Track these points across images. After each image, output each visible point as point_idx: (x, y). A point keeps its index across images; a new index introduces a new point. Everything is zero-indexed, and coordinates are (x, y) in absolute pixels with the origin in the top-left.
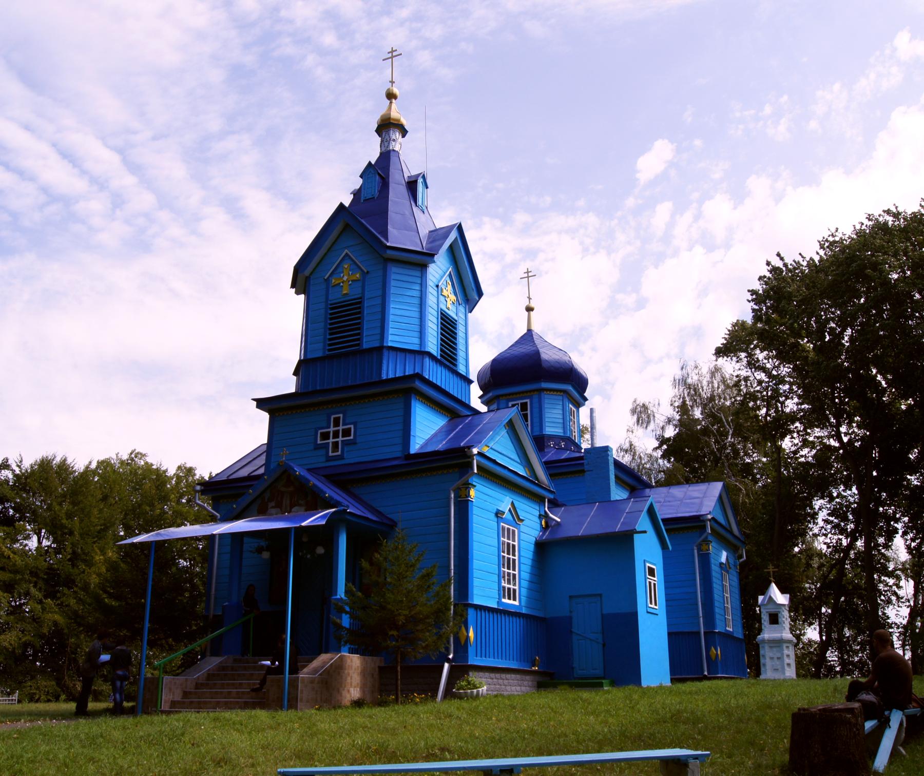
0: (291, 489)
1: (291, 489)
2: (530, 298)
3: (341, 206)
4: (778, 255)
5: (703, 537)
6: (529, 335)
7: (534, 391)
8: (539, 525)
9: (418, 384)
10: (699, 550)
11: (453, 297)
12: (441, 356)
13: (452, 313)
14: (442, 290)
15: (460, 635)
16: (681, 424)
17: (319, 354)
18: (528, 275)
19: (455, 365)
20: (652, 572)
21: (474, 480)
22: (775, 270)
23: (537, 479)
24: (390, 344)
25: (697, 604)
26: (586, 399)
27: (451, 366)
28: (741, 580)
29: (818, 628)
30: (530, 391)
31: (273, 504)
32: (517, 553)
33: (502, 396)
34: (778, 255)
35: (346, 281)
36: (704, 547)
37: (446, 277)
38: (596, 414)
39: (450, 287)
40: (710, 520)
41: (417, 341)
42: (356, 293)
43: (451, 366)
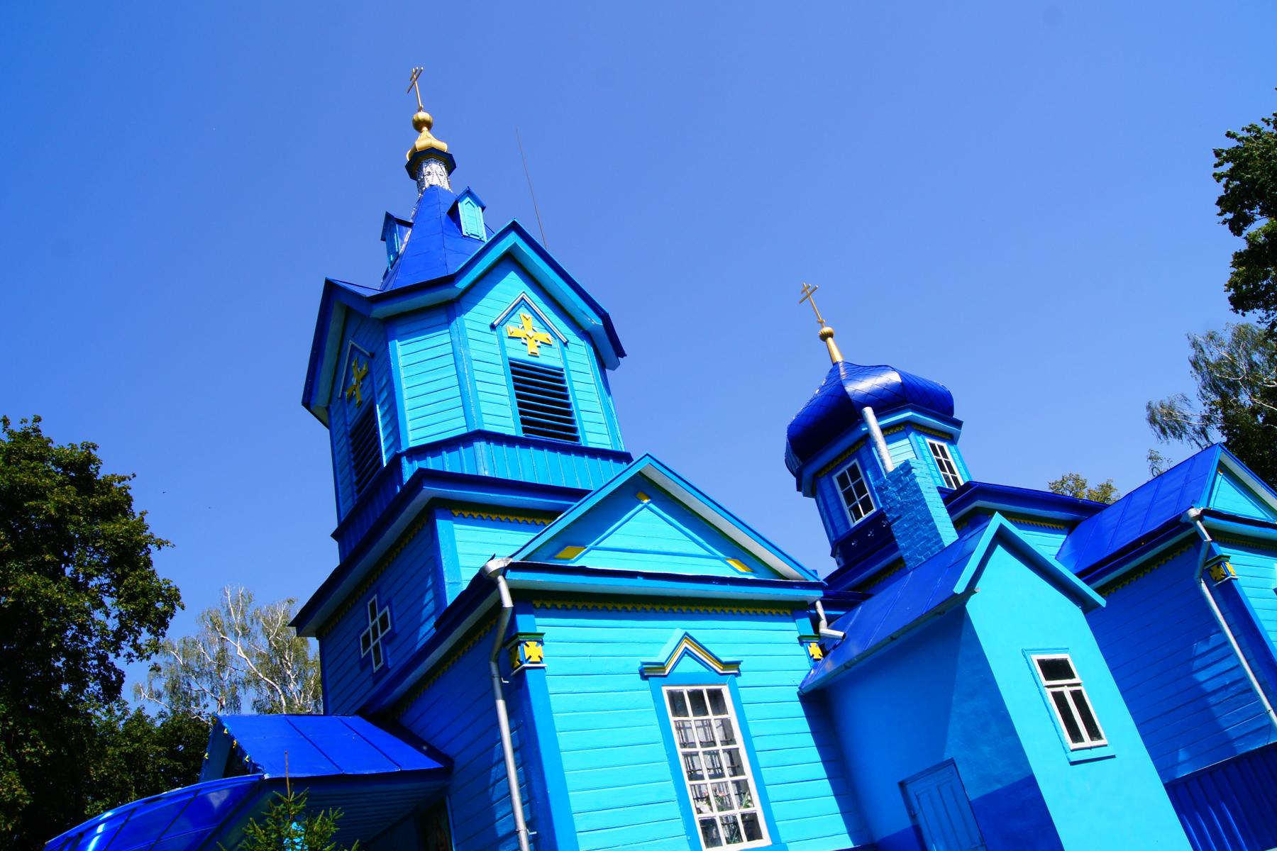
4: (1228, 135)
5: (1203, 552)
7: (857, 443)
8: (806, 659)
9: (431, 491)
12: (525, 430)
13: (550, 358)
16: (1229, 426)
20: (1055, 669)
21: (525, 623)
22: (1232, 155)
23: (781, 576)
24: (412, 445)
25: (1250, 689)
26: (958, 424)
27: (569, 442)
30: (853, 446)
32: (738, 735)
33: (820, 471)
34: (1228, 135)
40: (1200, 517)
43: (569, 442)
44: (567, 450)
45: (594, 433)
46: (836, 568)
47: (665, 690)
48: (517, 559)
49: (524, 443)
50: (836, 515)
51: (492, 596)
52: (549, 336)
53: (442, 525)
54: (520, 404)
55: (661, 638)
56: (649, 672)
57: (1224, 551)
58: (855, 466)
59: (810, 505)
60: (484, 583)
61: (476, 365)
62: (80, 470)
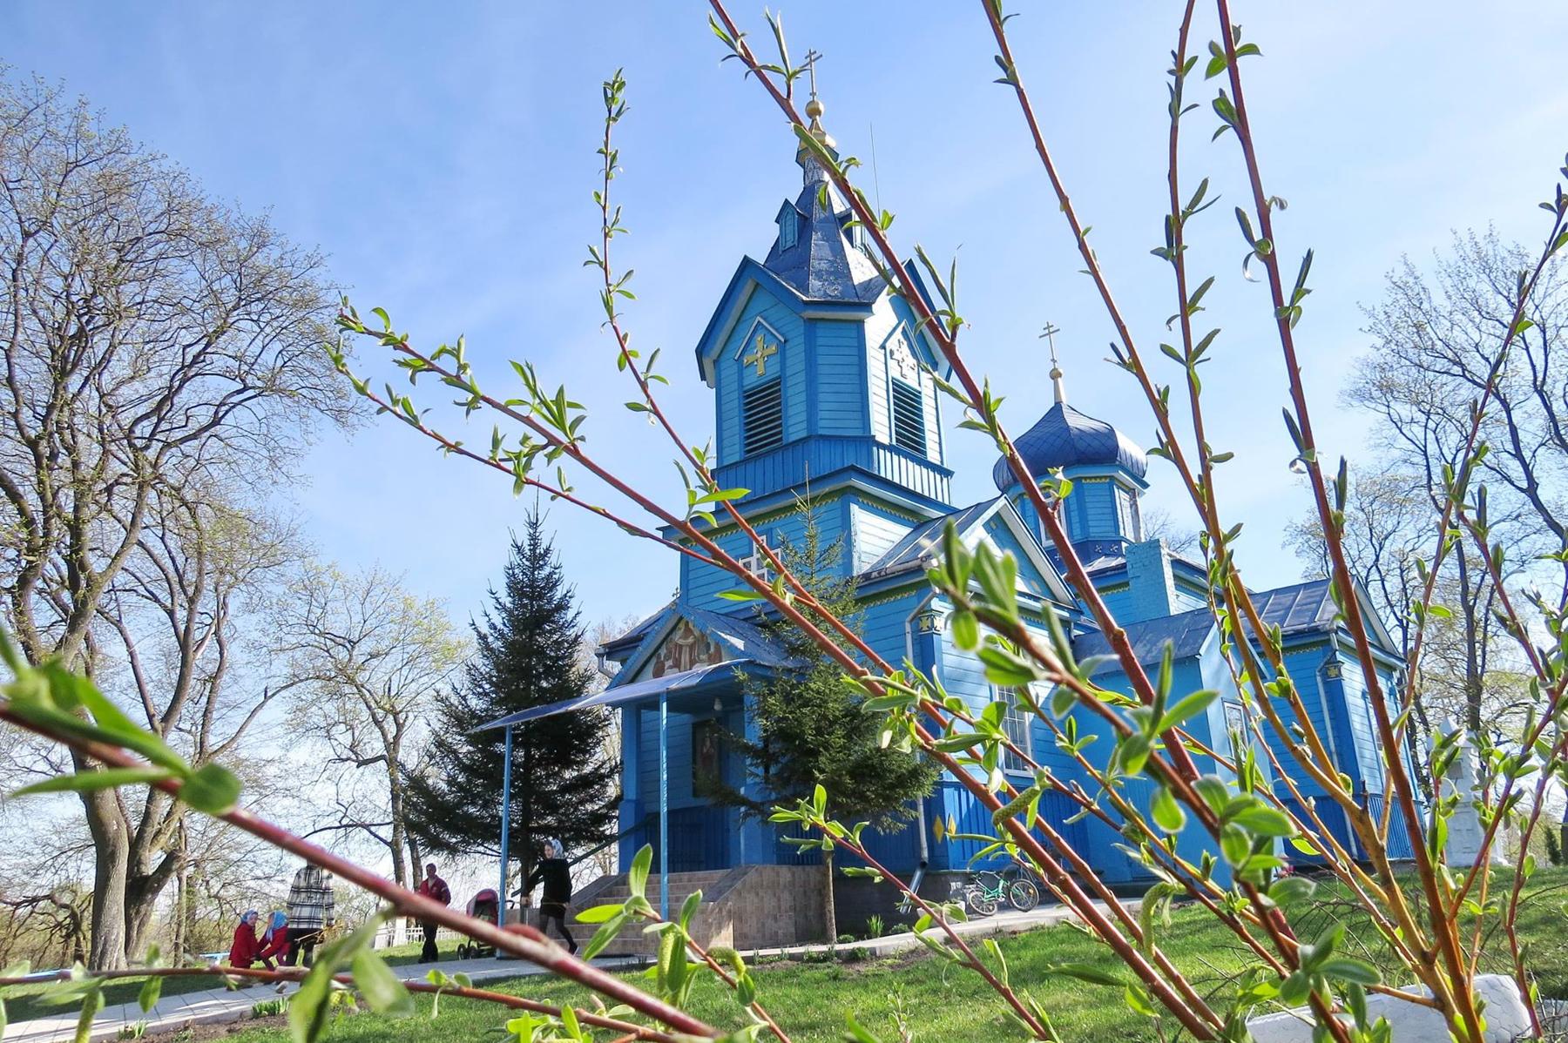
0: (691, 640)
1: (691, 640)
2: (1054, 361)
3: (747, 263)
6: (1056, 411)
10: (1325, 676)
11: (911, 361)
13: (911, 381)
14: (892, 352)
15: (936, 829)
17: (736, 458)
18: (1049, 331)
19: (924, 453)
24: (821, 432)
26: (1146, 485)
28: (849, 542)
29: (856, 562)
31: (669, 663)
35: (760, 362)
36: (1333, 672)
37: (898, 334)
38: (659, 355)
39: (905, 347)
41: (858, 424)
42: (774, 371)
49: (899, 452)
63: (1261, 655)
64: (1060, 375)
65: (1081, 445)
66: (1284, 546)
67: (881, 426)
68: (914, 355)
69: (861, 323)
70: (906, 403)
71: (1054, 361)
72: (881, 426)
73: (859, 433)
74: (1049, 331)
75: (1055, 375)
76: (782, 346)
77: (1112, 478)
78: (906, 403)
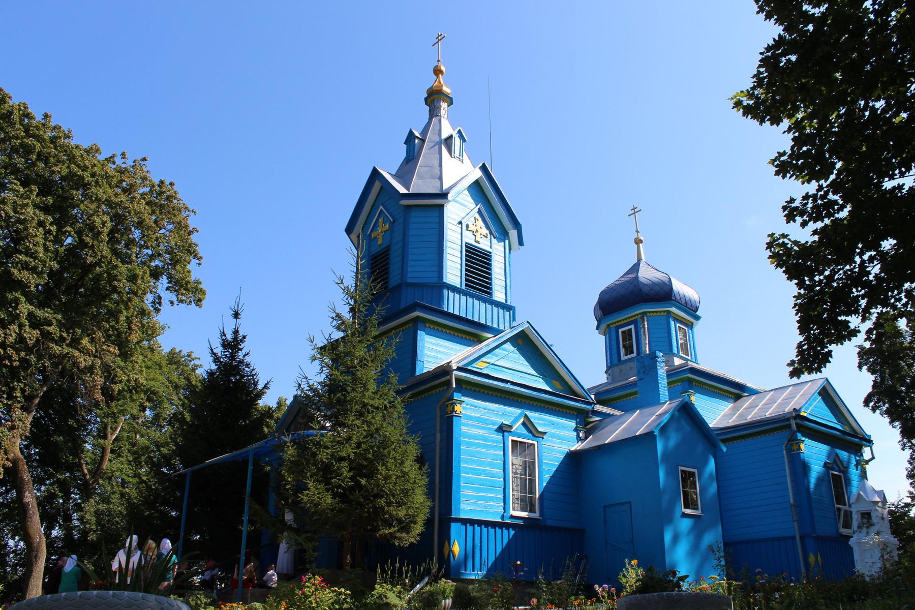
2: (637, 232)
6: (636, 268)
11: (485, 231)
14: (467, 226)
18: (635, 211)
19: (491, 294)
21: (457, 396)
26: (698, 318)
29: (419, 364)
39: (480, 223)
44: (485, 301)
45: (498, 295)
46: (606, 381)
47: (696, 471)
48: (460, 365)
49: (466, 294)
50: (615, 351)
51: (448, 378)
52: (488, 232)
53: (421, 335)
54: (490, 274)
55: (510, 414)
56: (503, 429)
57: (799, 436)
58: (630, 330)
59: (600, 341)
60: (445, 371)
61: (449, 244)
62: (163, 201)
63: (624, 346)
64: (641, 242)
65: (644, 289)
66: (46, 116)
67: (453, 271)
68: (488, 227)
69: (441, 207)
70: (478, 262)
71: (637, 232)
72: (453, 271)
73: (435, 280)
74: (635, 211)
75: (638, 242)
76: (392, 224)
77: (669, 312)
78: (478, 262)
